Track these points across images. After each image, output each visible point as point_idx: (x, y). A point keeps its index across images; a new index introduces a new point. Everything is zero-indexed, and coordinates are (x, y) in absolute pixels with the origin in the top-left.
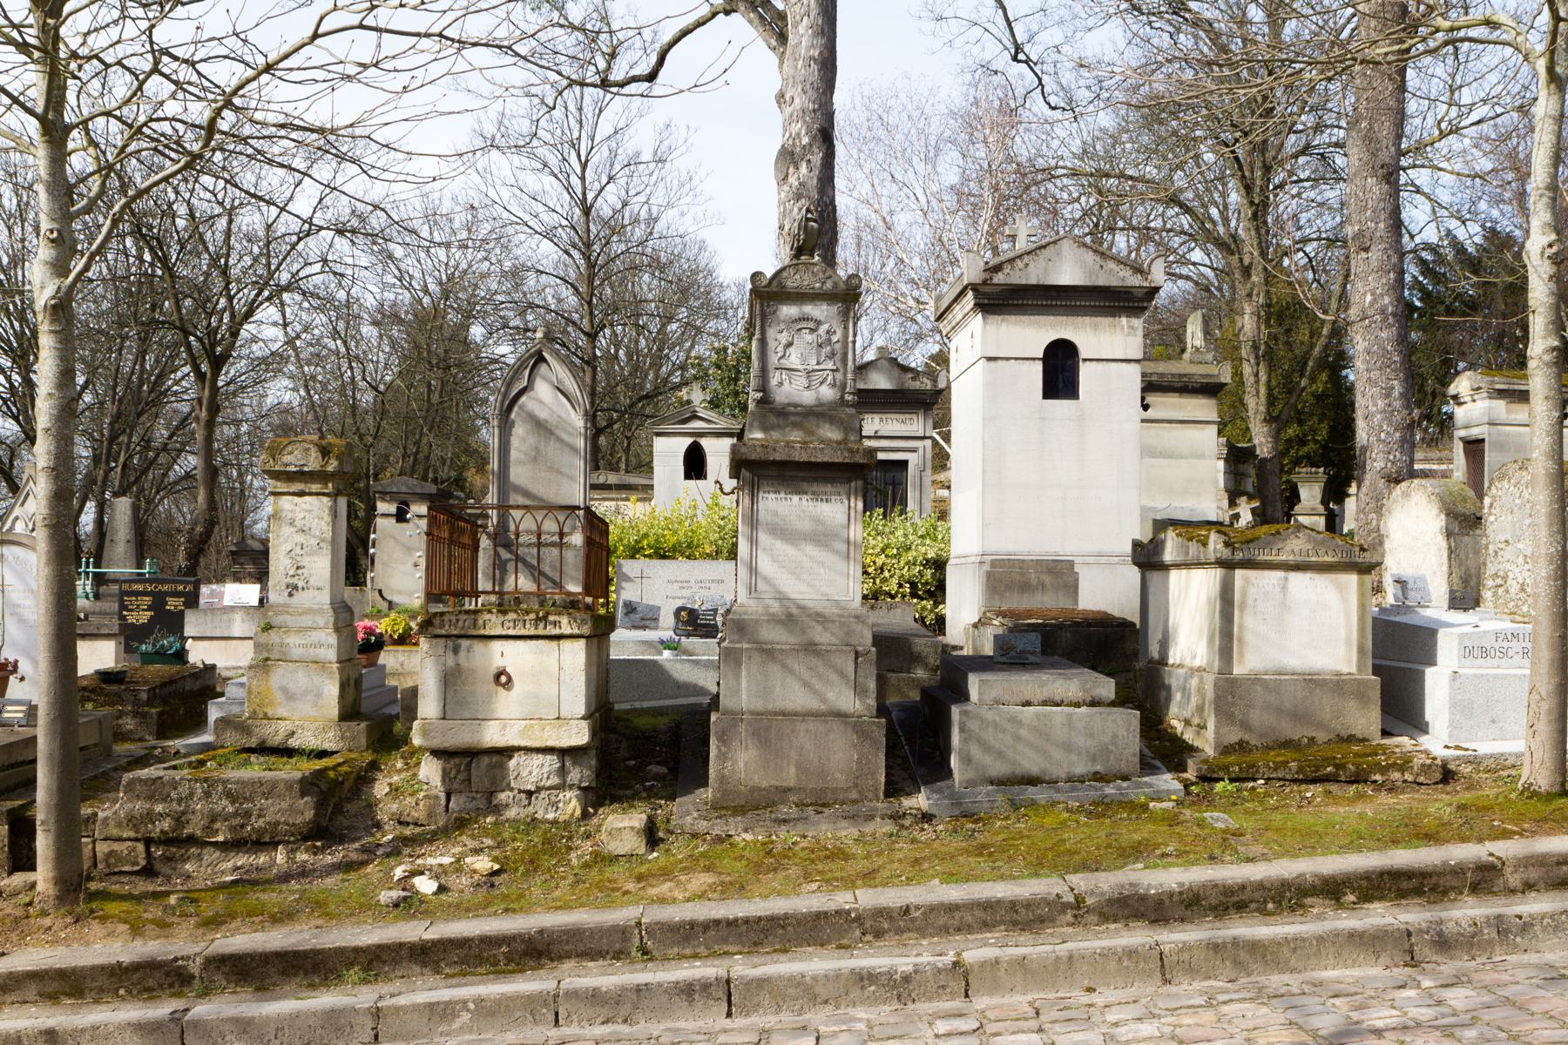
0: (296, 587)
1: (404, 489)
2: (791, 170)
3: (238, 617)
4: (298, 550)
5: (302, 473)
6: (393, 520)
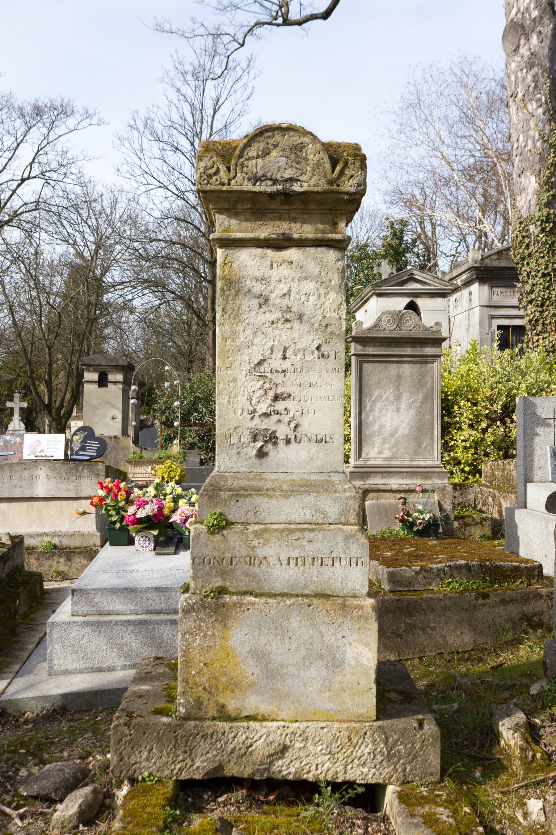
0: (272, 439)
1: (103, 363)
2: (522, 41)
3: (42, 473)
4: (276, 362)
5: (287, 196)
6: (96, 386)
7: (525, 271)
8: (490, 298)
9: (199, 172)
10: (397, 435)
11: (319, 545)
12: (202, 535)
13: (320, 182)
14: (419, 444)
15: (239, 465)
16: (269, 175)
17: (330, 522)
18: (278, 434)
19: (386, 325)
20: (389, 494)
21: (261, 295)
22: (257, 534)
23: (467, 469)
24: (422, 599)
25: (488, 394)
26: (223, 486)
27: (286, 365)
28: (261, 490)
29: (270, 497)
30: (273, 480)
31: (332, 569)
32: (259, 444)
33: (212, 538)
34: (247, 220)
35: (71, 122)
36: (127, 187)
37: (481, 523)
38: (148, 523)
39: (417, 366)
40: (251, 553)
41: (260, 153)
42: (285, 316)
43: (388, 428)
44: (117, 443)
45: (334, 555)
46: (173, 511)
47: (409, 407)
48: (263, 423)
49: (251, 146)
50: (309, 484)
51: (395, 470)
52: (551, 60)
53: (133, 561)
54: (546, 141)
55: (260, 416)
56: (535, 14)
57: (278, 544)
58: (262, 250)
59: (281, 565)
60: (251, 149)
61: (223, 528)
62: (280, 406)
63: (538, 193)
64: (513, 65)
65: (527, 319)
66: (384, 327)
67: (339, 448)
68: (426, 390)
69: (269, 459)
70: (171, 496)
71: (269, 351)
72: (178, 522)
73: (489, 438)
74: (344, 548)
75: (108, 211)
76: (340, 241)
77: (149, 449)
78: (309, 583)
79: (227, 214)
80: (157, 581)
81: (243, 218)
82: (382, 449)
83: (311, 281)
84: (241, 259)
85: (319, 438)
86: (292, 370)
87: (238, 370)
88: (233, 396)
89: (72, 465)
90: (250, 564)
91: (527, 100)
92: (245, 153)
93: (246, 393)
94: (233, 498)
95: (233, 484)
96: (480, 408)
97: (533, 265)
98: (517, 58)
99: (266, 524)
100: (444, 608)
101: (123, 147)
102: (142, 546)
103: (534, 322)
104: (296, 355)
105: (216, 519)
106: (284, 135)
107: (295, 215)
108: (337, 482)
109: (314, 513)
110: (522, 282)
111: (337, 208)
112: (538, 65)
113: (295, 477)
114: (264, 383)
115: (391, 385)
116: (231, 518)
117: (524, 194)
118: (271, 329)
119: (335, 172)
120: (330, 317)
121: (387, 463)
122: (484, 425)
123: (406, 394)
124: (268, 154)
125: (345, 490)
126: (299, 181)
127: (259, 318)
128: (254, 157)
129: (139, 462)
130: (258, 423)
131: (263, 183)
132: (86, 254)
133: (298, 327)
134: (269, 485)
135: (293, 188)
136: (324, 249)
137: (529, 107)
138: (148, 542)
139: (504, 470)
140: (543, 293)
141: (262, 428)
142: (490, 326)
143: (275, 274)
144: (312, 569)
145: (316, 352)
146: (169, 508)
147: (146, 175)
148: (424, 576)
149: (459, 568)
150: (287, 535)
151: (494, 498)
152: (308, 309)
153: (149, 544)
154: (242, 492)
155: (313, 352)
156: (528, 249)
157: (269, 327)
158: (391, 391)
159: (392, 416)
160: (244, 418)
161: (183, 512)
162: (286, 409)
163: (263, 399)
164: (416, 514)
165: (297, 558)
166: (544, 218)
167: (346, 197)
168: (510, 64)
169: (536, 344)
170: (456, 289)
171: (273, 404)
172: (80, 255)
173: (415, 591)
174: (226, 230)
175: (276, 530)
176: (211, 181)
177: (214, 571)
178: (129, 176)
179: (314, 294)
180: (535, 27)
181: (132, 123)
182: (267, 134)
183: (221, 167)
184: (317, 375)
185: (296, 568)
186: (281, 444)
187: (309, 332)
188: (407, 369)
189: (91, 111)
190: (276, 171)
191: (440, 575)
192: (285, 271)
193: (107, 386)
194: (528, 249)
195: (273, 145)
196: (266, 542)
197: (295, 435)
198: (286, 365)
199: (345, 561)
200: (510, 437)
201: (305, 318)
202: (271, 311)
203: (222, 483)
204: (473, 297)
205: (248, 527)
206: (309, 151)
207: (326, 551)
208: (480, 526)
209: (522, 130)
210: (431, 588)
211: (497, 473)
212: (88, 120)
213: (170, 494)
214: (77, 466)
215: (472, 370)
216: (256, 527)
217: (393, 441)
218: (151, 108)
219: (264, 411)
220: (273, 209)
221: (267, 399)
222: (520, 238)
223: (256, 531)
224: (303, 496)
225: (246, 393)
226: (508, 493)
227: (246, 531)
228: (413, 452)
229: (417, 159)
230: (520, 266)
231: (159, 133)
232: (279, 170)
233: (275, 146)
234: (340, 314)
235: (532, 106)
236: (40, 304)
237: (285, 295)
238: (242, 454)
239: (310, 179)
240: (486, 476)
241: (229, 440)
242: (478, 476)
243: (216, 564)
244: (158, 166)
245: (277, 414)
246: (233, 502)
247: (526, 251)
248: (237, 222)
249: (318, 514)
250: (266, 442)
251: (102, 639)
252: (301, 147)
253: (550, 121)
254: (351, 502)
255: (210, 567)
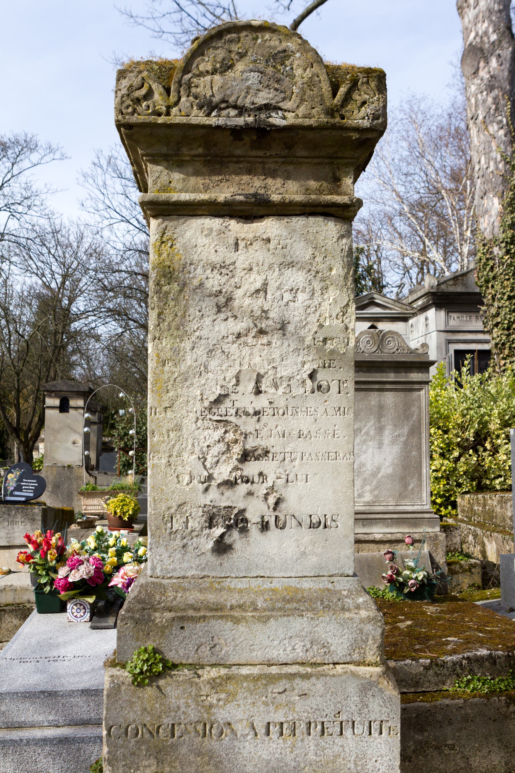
0: (239, 522)
1: (65, 388)
2: (482, 64)
6: (57, 411)
7: (490, 293)
8: (447, 323)
9: (120, 94)
10: (380, 475)
11: (317, 699)
12: (123, 688)
13: (314, 111)
14: (405, 486)
15: (185, 565)
16: (232, 100)
17: (336, 661)
18: (248, 515)
19: (365, 347)
20: (372, 546)
21: (220, 292)
22: (215, 685)
23: (439, 501)
24: (436, 707)
25: (459, 422)
26: (159, 603)
27: (261, 402)
28: (221, 609)
29: (237, 621)
30: (240, 591)
31: (339, 740)
32: (218, 531)
33: (140, 692)
34: (197, 173)
35: (35, 157)
36: (92, 222)
37: (470, 570)
38: (82, 588)
39: (401, 394)
40: (206, 716)
41: (218, 65)
42: (259, 325)
43: (369, 467)
44: (71, 472)
45: (343, 717)
46: (117, 568)
47: (393, 442)
48: (224, 498)
49: (203, 55)
50: (299, 596)
51: (377, 516)
52: (511, 83)
53: (61, 640)
54: (508, 162)
55: (219, 485)
56: (494, 37)
57: (249, 701)
58: (221, 220)
59: (256, 735)
60: (203, 60)
61: (160, 675)
62: (251, 469)
63: (502, 215)
64: (473, 88)
65: (493, 342)
66: (363, 349)
67: (346, 537)
68: (412, 423)
69: (235, 555)
70: (114, 549)
71: (234, 381)
72: (120, 586)
73: (462, 468)
74: (360, 706)
75: (75, 245)
76: (345, 207)
77: (109, 473)
78: (302, 765)
79: (165, 164)
80: (86, 678)
81: (191, 170)
82: (362, 492)
83: (299, 269)
84: (188, 234)
85: (314, 521)
86: (271, 412)
87: (184, 412)
88: (175, 454)
89: (4, 509)
90: (204, 735)
91: (488, 121)
92: (194, 66)
93: (197, 449)
94: (175, 623)
95: (175, 598)
96: (451, 436)
97: (498, 287)
98: (477, 81)
99: (230, 666)
100: (466, 719)
101: (87, 184)
102: (76, 617)
103: (501, 346)
104: (276, 387)
105: (147, 660)
106: (256, 38)
107: (273, 166)
108: (345, 593)
109: (308, 646)
110: (487, 305)
111: (340, 154)
112: (498, 87)
113: (276, 584)
114: (226, 432)
115: (372, 417)
116: (172, 656)
117: (487, 216)
118: (236, 345)
119: (338, 96)
120: (330, 326)
121: (368, 508)
122: (456, 454)
123: (389, 427)
124: (231, 67)
125: (358, 607)
126: (281, 109)
127: (217, 329)
128: (208, 72)
129: (92, 493)
130: (216, 497)
131: (224, 113)
132: (53, 285)
133: (279, 343)
134: (234, 600)
135: (270, 120)
136: (320, 219)
137: (491, 129)
138: (83, 611)
139: (485, 505)
140: (509, 316)
141: (223, 505)
142: (447, 351)
143: (242, 258)
144: (306, 742)
145: (309, 382)
146: (111, 563)
147: (108, 210)
148: (436, 673)
149: (480, 660)
150: (266, 685)
151: (475, 536)
152: (295, 313)
153: (84, 613)
154: (191, 613)
155: (304, 382)
156: (492, 271)
157: (234, 342)
158: (372, 423)
159: (373, 453)
160: (193, 489)
161: (125, 574)
162: (261, 474)
163: (224, 457)
164: (407, 572)
165: (282, 724)
166: (509, 240)
167: (355, 136)
168: (470, 87)
169: (503, 368)
170: (414, 315)
171: (240, 466)
172: (48, 287)
173: (424, 692)
174: (164, 189)
175: (246, 677)
176: (139, 109)
177: (143, 747)
178: (93, 211)
179: (303, 291)
180: (494, 51)
181: (96, 161)
182: (229, 36)
183: (154, 86)
184: (310, 419)
185: (281, 741)
186: (254, 530)
187: (297, 350)
188: (390, 398)
189: (54, 146)
190: (243, 94)
191: (456, 670)
192: (257, 254)
193: (68, 412)
194: (492, 271)
195: (239, 53)
196: (230, 698)
197: (276, 517)
198: (261, 402)
199: (361, 727)
200: (483, 466)
201: (290, 328)
202: (236, 317)
203: (158, 597)
204: (429, 322)
205: (200, 672)
206: (296, 63)
207: (330, 710)
208: (468, 573)
209: (483, 152)
210: (445, 688)
211: (476, 508)
212: (51, 155)
213: (114, 546)
214: (9, 510)
215: (440, 396)
216: (214, 673)
217: (374, 483)
218: (114, 147)
219: (225, 476)
220: (239, 156)
221: (231, 457)
222: (484, 261)
223: (214, 680)
224: (291, 618)
225: (197, 449)
226: (493, 531)
227: (197, 680)
228: (398, 495)
229: (368, 192)
230: (484, 288)
231: (122, 171)
232: (247, 93)
233: (242, 56)
234: (347, 321)
235: (493, 128)
236: (9, 332)
237: (257, 291)
238: (191, 548)
239: (298, 107)
240: (463, 511)
241: (169, 525)
242: (450, 508)
243: (147, 736)
244: (120, 201)
245: (247, 482)
246: (175, 630)
247: (490, 273)
248: (182, 176)
249: (315, 648)
250: (229, 528)
251: (8, 764)
252: (284, 56)
253: (511, 142)
254: (369, 627)
255: (137, 742)
